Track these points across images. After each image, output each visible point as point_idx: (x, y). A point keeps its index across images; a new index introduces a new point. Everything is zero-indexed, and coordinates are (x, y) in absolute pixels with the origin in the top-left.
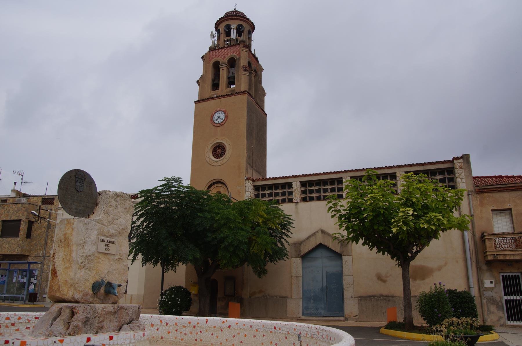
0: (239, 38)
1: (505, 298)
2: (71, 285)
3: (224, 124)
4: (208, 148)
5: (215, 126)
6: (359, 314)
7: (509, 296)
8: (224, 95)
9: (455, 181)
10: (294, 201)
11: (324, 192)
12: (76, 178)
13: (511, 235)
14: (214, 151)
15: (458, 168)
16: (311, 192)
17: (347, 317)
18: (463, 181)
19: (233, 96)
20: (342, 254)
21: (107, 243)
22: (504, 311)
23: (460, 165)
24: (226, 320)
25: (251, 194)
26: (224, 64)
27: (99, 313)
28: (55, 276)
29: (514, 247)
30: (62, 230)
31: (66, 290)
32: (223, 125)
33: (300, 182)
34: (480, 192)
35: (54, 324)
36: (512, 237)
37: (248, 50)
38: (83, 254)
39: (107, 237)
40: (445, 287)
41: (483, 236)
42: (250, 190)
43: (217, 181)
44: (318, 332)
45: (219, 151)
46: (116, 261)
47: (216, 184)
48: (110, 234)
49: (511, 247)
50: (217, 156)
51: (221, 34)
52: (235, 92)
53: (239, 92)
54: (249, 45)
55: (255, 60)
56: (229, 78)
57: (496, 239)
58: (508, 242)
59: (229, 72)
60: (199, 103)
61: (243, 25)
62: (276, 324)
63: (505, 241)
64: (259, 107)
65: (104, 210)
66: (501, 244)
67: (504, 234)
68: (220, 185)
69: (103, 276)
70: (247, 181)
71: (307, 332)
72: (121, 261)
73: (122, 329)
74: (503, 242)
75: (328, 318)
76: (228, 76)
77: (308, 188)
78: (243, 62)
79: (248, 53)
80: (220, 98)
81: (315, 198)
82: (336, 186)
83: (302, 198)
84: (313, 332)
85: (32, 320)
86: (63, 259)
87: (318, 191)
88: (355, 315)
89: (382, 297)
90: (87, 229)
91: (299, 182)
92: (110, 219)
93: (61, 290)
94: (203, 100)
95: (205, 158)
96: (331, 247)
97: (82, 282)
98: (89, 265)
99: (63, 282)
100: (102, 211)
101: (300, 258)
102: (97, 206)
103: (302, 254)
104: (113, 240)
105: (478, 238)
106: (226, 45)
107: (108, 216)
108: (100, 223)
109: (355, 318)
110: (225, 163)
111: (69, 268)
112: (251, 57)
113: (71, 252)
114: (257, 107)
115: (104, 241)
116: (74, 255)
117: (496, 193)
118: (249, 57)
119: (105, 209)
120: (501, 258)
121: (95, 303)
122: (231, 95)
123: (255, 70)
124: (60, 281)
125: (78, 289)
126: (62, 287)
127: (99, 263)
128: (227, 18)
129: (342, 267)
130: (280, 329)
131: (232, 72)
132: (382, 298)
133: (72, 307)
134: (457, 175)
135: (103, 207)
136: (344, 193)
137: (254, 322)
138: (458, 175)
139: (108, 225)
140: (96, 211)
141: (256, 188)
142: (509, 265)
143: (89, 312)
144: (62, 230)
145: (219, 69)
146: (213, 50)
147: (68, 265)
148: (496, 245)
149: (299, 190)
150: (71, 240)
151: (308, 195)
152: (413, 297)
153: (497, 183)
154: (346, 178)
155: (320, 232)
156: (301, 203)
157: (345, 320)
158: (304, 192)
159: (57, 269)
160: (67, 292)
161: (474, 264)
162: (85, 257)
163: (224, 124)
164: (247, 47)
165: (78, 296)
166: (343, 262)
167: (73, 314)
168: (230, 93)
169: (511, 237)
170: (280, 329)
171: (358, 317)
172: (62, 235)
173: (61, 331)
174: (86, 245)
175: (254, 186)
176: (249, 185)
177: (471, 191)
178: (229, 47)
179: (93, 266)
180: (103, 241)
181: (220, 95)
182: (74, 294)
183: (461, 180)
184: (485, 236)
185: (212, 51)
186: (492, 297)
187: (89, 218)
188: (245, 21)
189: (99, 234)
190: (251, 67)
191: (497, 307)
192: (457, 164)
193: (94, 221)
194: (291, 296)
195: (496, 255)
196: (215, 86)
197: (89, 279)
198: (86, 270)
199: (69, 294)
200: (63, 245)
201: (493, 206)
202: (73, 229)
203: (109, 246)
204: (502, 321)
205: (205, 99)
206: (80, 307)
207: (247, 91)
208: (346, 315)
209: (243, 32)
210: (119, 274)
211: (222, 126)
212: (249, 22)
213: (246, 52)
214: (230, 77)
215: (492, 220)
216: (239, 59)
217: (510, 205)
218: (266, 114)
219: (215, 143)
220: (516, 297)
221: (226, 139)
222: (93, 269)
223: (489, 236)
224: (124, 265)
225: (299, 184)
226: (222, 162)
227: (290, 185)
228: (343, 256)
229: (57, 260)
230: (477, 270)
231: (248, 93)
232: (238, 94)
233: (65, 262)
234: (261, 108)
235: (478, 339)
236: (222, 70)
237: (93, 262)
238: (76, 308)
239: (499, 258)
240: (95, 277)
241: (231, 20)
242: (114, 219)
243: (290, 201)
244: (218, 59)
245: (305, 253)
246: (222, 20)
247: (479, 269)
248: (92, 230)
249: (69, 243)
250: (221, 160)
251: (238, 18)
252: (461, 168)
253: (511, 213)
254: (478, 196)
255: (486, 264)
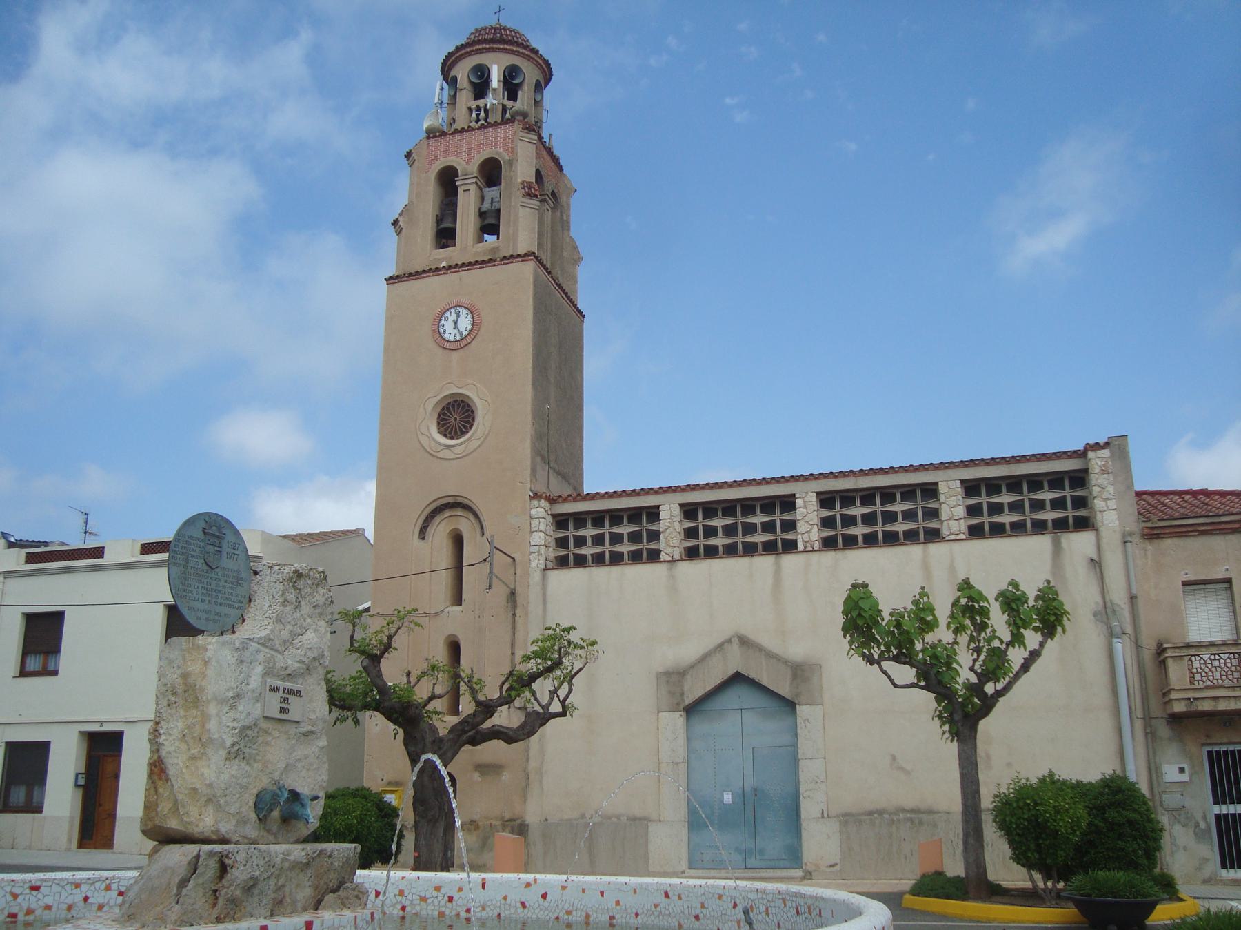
0: (509, 103)
1: (1217, 809)
2: (209, 800)
3: (469, 343)
4: (425, 410)
5: (446, 349)
6: (840, 860)
7: (1234, 803)
8: (470, 264)
9: (1090, 506)
10: (663, 556)
11: (745, 533)
12: (205, 533)
13: (1230, 647)
14: (442, 416)
15: (1097, 471)
16: (711, 532)
17: (810, 868)
18: (1110, 508)
19: (495, 265)
20: (796, 702)
21: (284, 696)
22: (1211, 838)
23: (1104, 465)
24: (536, 880)
25: (548, 537)
26: (467, 177)
27: (276, 866)
28: (160, 779)
29: (1237, 679)
30: (175, 665)
31: (194, 811)
32: (466, 345)
33: (681, 505)
34: (1155, 536)
35: (183, 894)
36: (1233, 653)
37: (536, 138)
38: (235, 724)
39: (283, 680)
40: (1031, 779)
41: (1160, 650)
42: (542, 527)
43: (451, 500)
44: (784, 900)
45: (455, 419)
46: (302, 738)
47: (447, 511)
48: (289, 673)
49: (1231, 677)
50: (450, 433)
51: (461, 90)
52: (502, 256)
53: (512, 256)
54: (536, 122)
55: (553, 164)
56: (482, 214)
57: (1193, 658)
58: (1223, 665)
59: (482, 199)
60: (399, 282)
61: (521, 67)
62: (670, 885)
63: (1216, 663)
64: (564, 296)
65: (271, 612)
66: (1207, 670)
67: (1212, 644)
68: (460, 512)
69: (276, 776)
70: (535, 502)
71: (753, 901)
72: (312, 737)
73: (323, 904)
74: (1210, 666)
75: (759, 872)
76: (480, 209)
77: (701, 522)
78: (522, 170)
79: (536, 147)
80: (459, 271)
81: (721, 549)
82: (778, 516)
83: (684, 548)
84: (771, 900)
85: (21, 894)
86: (184, 735)
87: (730, 530)
88: (832, 863)
89: (901, 815)
90: (242, 662)
91: (678, 505)
92: (285, 634)
93: (181, 813)
94: (410, 274)
95: (417, 436)
96: (765, 683)
97: (234, 792)
98: (248, 750)
99: (186, 792)
100: (267, 615)
101: (682, 713)
102: (252, 603)
103: (688, 701)
104: (295, 687)
105: (1148, 655)
106: (474, 123)
107: (282, 627)
108: (267, 647)
109: (830, 872)
110: (471, 453)
111: (200, 758)
112: (543, 158)
113: (205, 717)
114: (558, 295)
115: (278, 689)
116: (212, 725)
117: (1192, 538)
118: (538, 156)
119: (274, 611)
120: (1207, 706)
121: (261, 842)
122: (488, 262)
123: (553, 193)
124: (178, 792)
125: (227, 809)
126: (184, 806)
127: (267, 743)
128: (478, 47)
129: (796, 735)
130: (680, 898)
131: (492, 198)
132: (902, 816)
133: (220, 852)
134: (1096, 490)
135: (267, 605)
136: (799, 536)
137: (609, 883)
138: (1098, 489)
139: (284, 649)
140: (250, 615)
141: (561, 522)
142: (1224, 725)
143: (257, 865)
144: (175, 665)
145: (456, 188)
146: (438, 134)
147: (196, 750)
148: (1193, 674)
149: (678, 527)
150: (204, 690)
151: (701, 542)
152: (985, 811)
153: (1196, 513)
154: (806, 496)
155: (736, 640)
156: (684, 562)
157: (804, 878)
158: (691, 533)
159: (168, 761)
160: (199, 817)
161: (1139, 724)
162: (239, 731)
163: (469, 343)
164: (535, 132)
165: (225, 828)
166: (798, 723)
167: (223, 869)
168: (486, 258)
169: (1231, 653)
170: (680, 898)
171: (838, 868)
172: (176, 676)
173: (200, 911)
174: (241, 701)
175: (554, 516)
176: (540, 511)
177: (1131, 534)
178: (482, 127)
179: (256, 751)
180: (275, 689)
181: (459, 263)
182: (216, 822)
183: (1106, 504)
184: (1164, 650)
185: (435, 137)
186: (1183, 807)
187: (234, 632)
188: (528, 58)
189: (265, 675)
190: (544, 185)
191: (1196, 834)
192: (1097, 460)
193: (255, 642)
194: (660, 815)
195: (1195, 699)
196: (445, 236)
197: (248, 783)
198: (241, 763)
199: (206, 822)
200: (181, 701)
201: (1187, 571)
202: (206, 663)
203: (287, 703)
204: (1207, 872)
205: (417, 272)
206: (237, 852)
207: (534, 253)
208: (808, 864)
209: (519, 85)
210: (308, 770)
211: (466, 348)
212: (536, 58)
213: (530, 144)
214: (485, 213)
215: (1183, 608)
216: (511, 163)
217: (1227, 570)
218: (581, 313)
219: (445, 395)
220: (1220, 806)
221: (478, 385)
222: (255, 760)
223: (1177, 650)
224: (318, 746)
225: (676, 510)
226: (466, 448)
227: (653, 514)
228: (797, 706)
229: (167, 740)
230: (1147, 738)
231: (537, 258)
232: (509, 259)
233: (188, 745)
234: (568, 297)
235: (1151, 913)
236: (464, 191)
237: (255, 743)
238: (230, 855)
239: (1200, 708)
240: (260, 779)
241: (489, 52)
242: (294, 635)
243: (654, 556)
244: (451, 161)
245: (697, 699)
246: (463, 52)
247: (1150, 735)
248: (251, 663)
249: (197, 697)
250: (462, 444)
251: (508, 47)
252: (1104, 471)
253: (1231, 588)
254: (1149, 547)
255: (1169, 723)
